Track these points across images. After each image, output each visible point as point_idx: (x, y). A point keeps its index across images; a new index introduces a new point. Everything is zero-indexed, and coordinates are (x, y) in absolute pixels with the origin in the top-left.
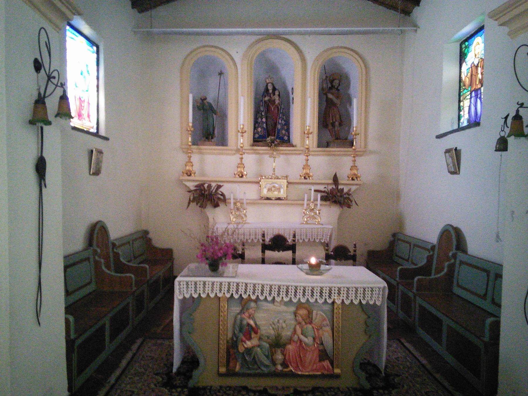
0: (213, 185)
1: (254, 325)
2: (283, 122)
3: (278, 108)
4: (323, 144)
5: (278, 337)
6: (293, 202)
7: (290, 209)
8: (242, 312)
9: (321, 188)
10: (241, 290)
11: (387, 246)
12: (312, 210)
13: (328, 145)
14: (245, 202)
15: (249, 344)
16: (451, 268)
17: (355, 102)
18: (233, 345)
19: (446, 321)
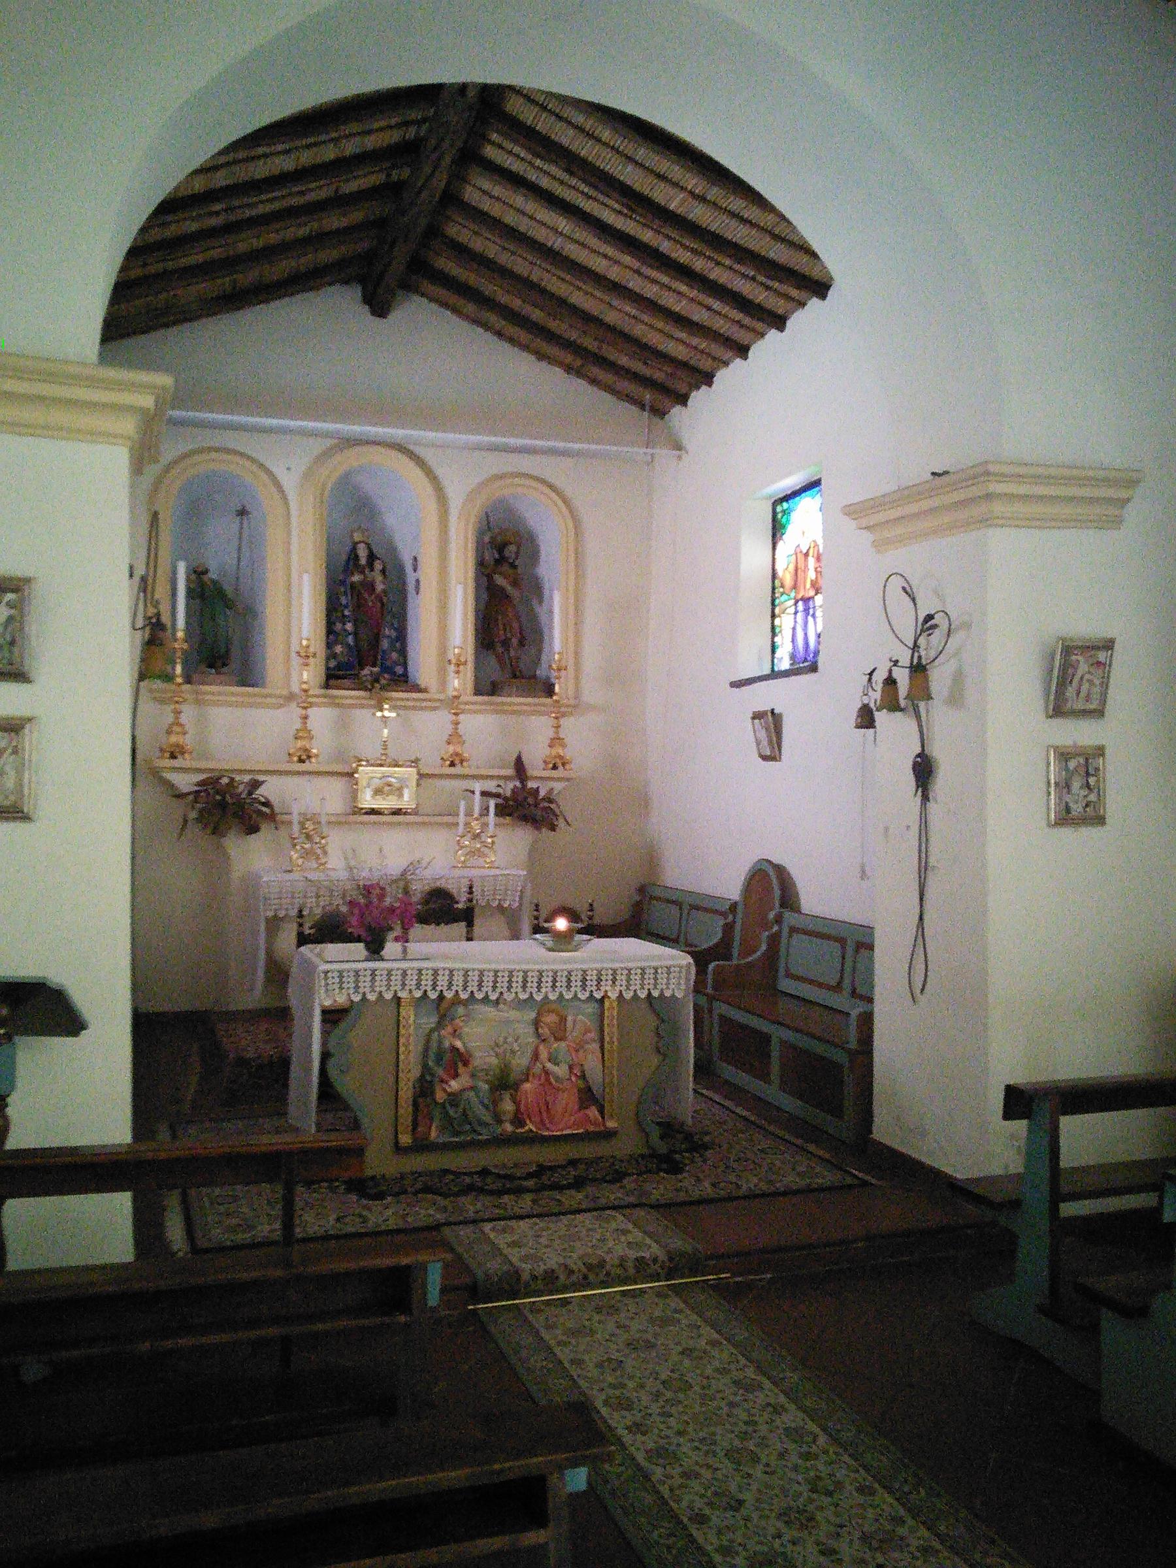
1: (462, 1050)
2: (394, 634)
3: (381, 601)
4: (487, 687)
5: (505, 1070)
6: (426, 819)
7: (421, 835)
8: (440, 1025)
9: (491, 786)
10: (443, 982)
12: (476, 837)
14: (324, 819)
15: (455, 1085)
16: (774, 940)
17: (557, 598)
18: (424, 1088)
19: (779, 1034)
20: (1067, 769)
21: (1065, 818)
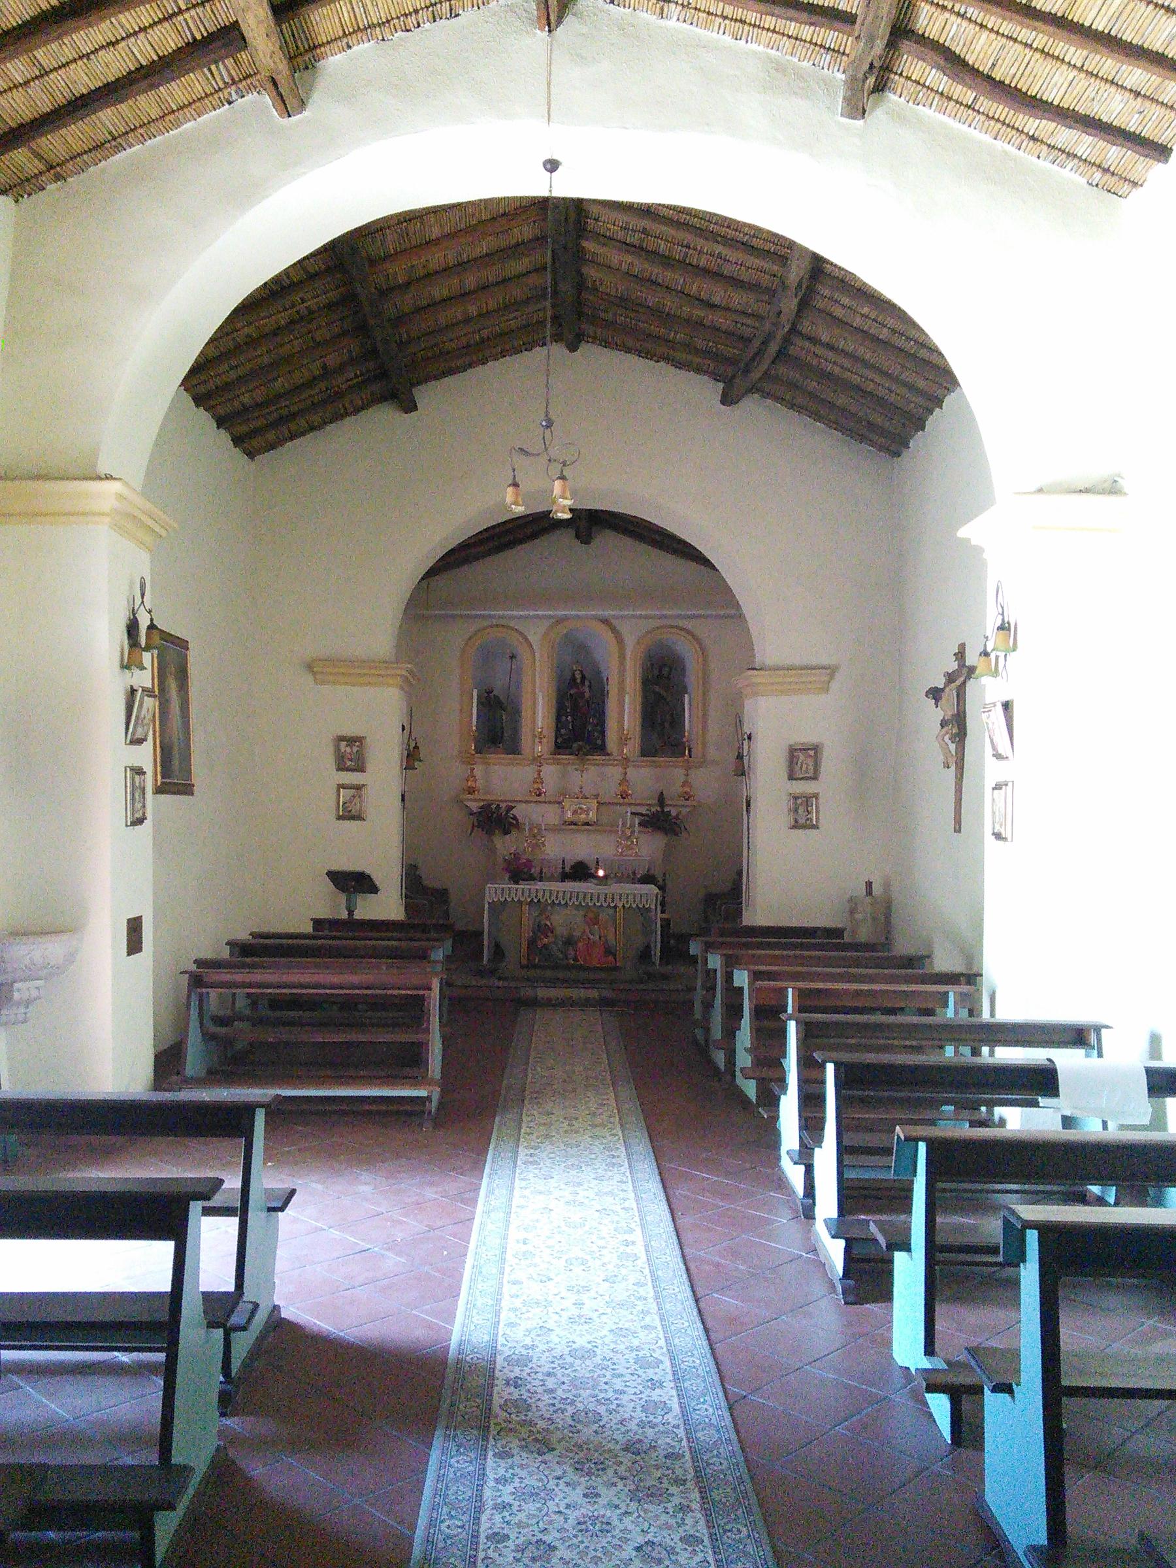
0: (503, 805)
4: (647, 752)
9: (643, 810)
11: (730, 885)
13: (653, 754)
18: (532, 942)
20: (796, 803)
21: (796, 826)
